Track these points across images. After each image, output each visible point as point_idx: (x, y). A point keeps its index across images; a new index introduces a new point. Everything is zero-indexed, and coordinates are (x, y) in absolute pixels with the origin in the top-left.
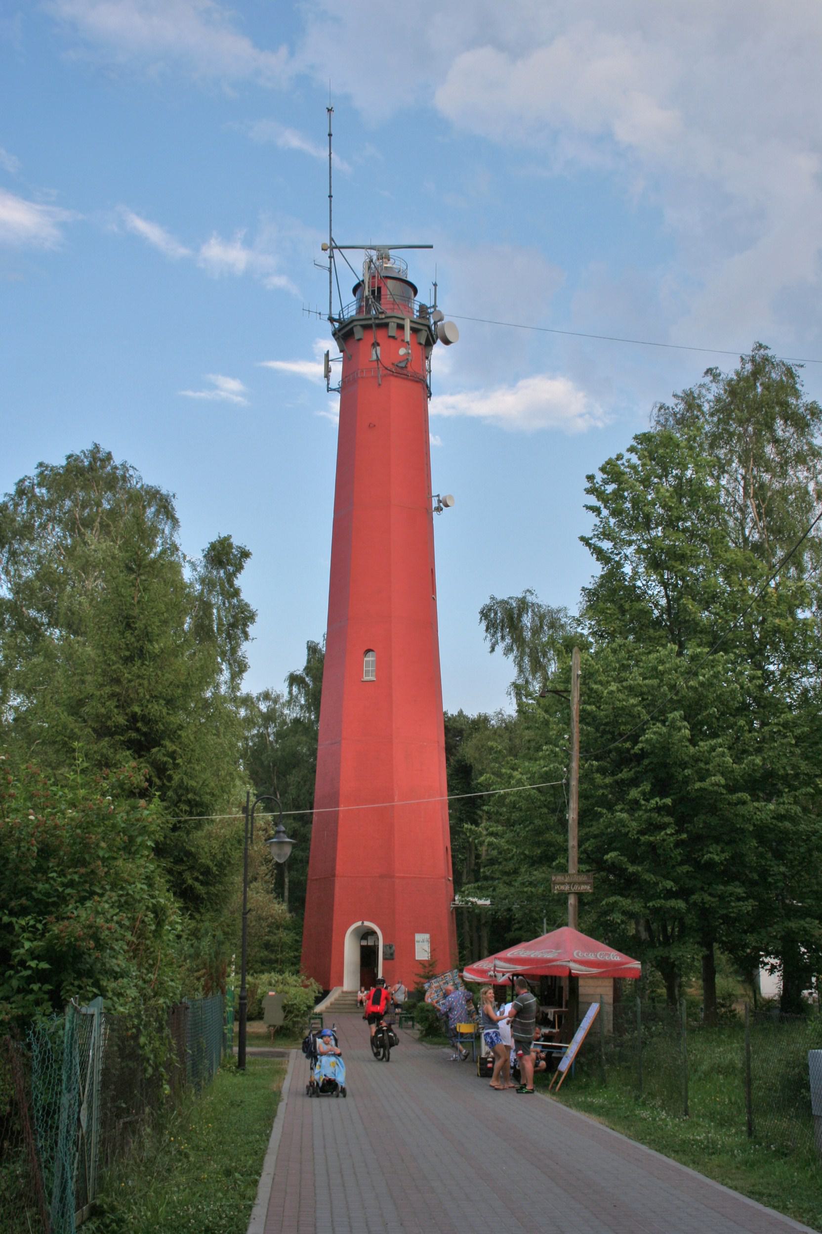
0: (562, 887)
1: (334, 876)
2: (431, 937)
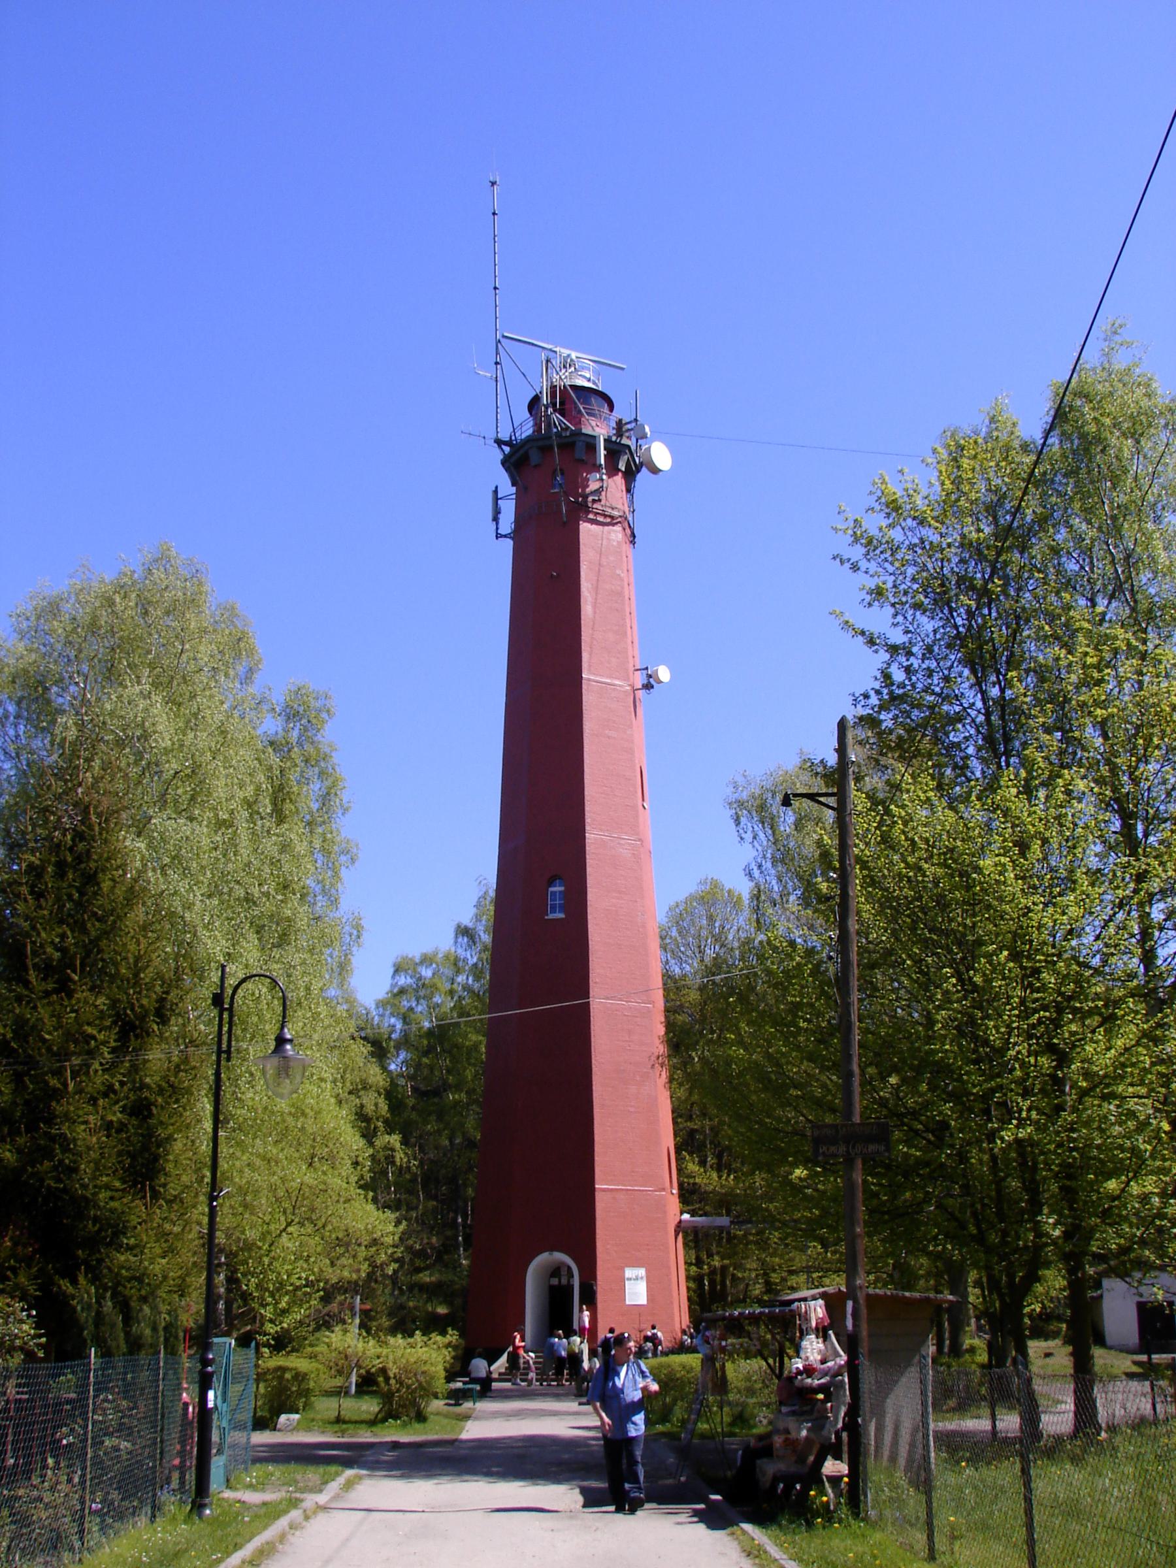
2: (647, 1272)
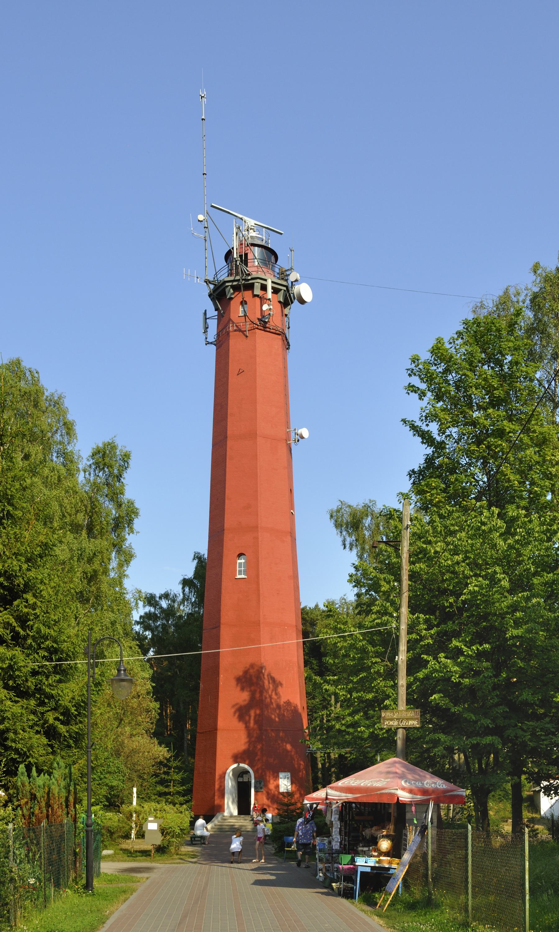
0: (391, 723)
1: (216, 729)
